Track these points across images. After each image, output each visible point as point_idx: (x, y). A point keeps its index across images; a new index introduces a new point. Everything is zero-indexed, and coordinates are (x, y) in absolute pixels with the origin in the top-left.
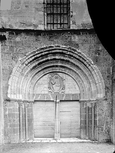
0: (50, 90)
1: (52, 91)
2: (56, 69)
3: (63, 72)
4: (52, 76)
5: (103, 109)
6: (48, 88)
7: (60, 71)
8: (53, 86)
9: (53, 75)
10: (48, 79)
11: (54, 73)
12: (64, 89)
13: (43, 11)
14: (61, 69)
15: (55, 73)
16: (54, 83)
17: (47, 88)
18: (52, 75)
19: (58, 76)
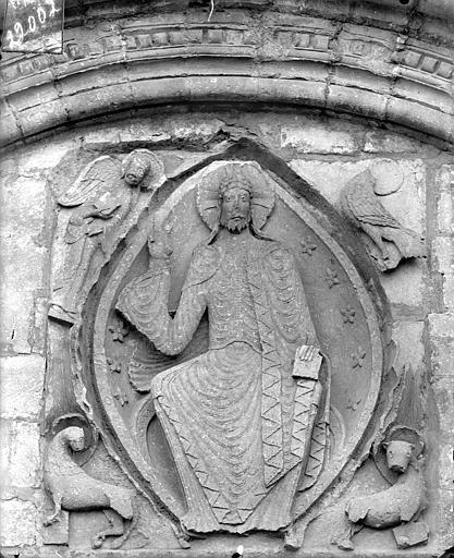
0: (81, 484)
1: (121, 497)
2: (233, 44)
3: (378, 100)
4: (138, 185)
5: (270, 475)
6: (51, 426)
7: (314, 86)
8: (166, 384)
9: (163, 167)
10: (46, 238)
11: (181, 131)
12: (399, 451)
13: (305, 327)
14: (320, 48)
15: (206, 129)
16: (169, 336)
17: (30, 438)
18: (138, 161)
19: (272, 188)
